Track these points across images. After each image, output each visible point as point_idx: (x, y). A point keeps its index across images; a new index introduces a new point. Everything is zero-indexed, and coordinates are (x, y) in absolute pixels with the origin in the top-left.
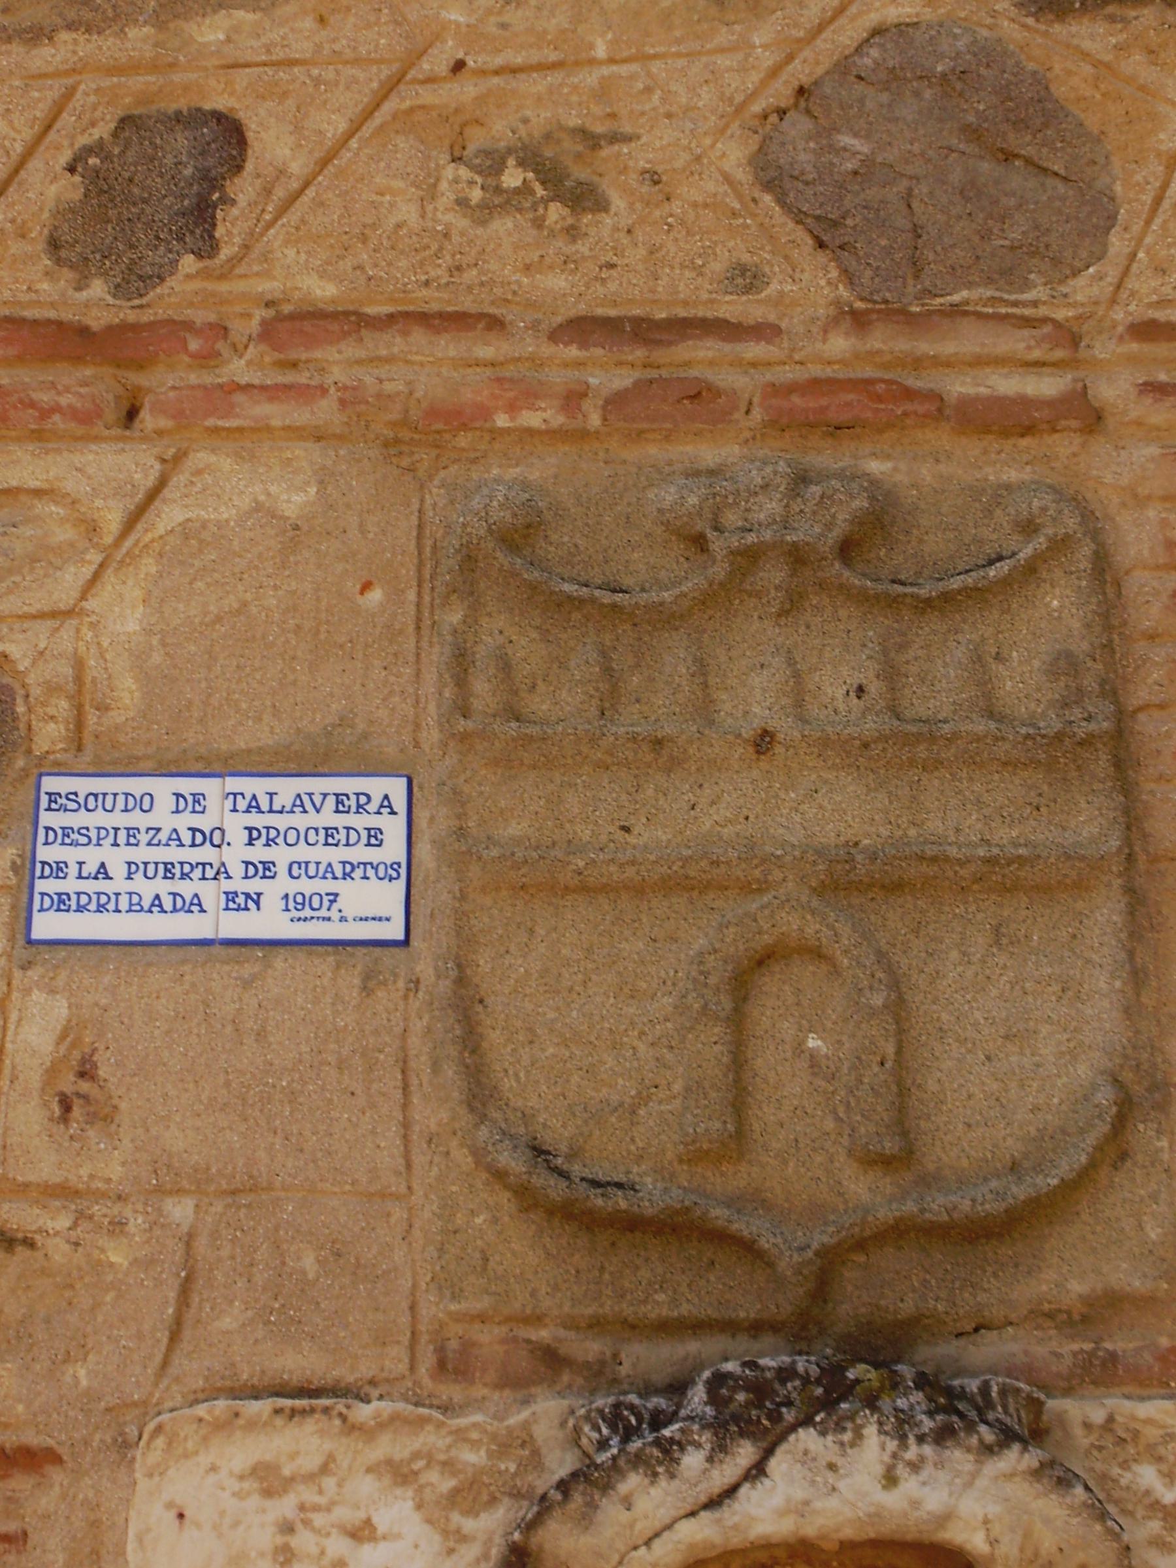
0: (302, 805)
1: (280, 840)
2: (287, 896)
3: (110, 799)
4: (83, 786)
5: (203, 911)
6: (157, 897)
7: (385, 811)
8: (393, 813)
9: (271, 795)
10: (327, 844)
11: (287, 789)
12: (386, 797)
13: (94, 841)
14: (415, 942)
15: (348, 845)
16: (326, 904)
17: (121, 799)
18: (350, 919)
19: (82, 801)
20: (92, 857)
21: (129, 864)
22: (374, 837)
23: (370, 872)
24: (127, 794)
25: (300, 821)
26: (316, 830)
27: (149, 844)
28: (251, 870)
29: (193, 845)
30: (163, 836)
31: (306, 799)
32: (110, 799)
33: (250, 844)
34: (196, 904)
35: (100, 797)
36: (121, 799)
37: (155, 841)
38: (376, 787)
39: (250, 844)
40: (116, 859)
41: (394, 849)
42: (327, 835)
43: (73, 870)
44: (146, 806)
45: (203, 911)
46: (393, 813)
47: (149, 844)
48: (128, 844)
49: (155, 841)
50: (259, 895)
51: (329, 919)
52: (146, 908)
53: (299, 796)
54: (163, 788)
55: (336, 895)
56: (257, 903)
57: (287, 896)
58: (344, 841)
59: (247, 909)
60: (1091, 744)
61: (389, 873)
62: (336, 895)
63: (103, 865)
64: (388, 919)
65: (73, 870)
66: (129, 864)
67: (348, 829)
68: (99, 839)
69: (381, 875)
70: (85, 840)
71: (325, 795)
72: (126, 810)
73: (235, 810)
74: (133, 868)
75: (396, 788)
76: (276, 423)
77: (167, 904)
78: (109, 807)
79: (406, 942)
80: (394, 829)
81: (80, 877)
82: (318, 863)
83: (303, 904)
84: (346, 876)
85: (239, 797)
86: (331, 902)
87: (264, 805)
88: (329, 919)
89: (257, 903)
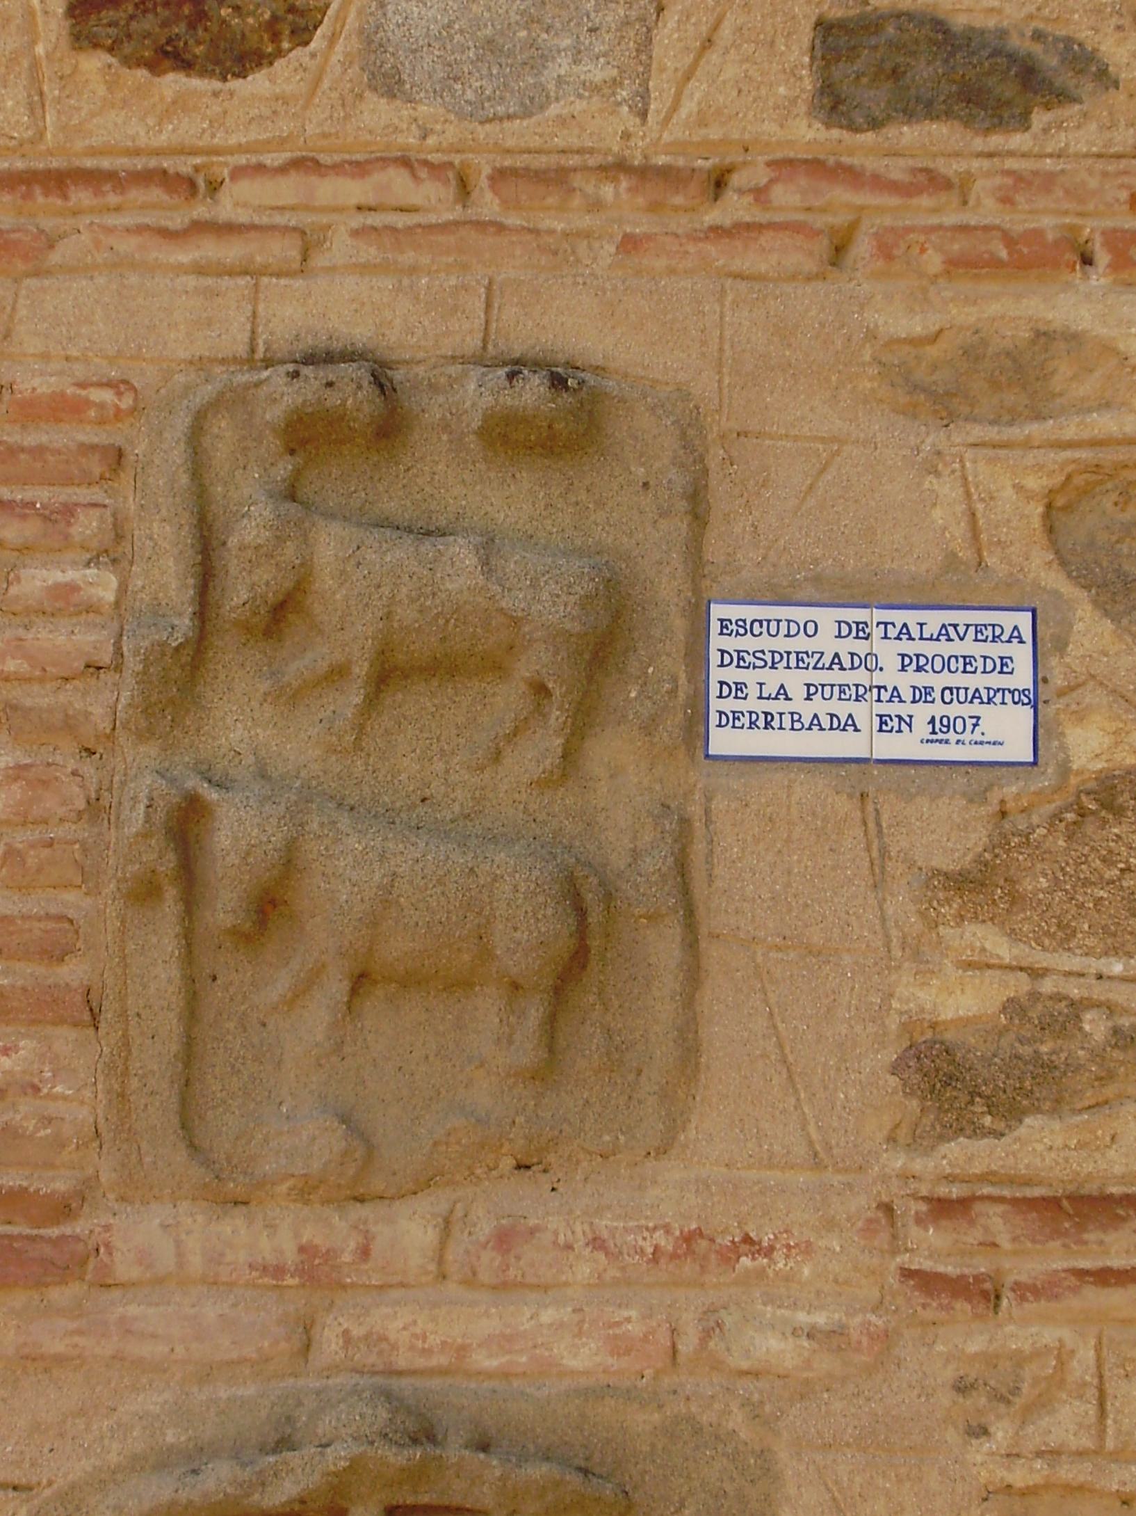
0: (947, 634)
1: (928, 667)
2: (933, 718)
3: (773, 625)
4: (750, 612)
5: (856, 730)
6: (815, 716)
7: (904, 637)
8: (1021, 642)
9: (921, 625)
10: (965, 671)
11: (934, 620)
12: (1016, 628)
13: (770, 664)
14: (1040, 761)
15: (984, 672)
16: (969, 727)
17: (783, 625)
18: (967, 742)
19: (748, 627)
20: (772, 680)
21: (808, 685)
22: (1004, 665)
23: (1008, 696)
24: (789, 621)
25: (945, 648)
26: (956, 657)
27: (815, 668)
28: (726, 690)
29: (852, 668)
30: (826, 660)
31: (951, 629)
32: (773, 625)
33: (903, 669)
34: (851, 723)
35: (765, 624)
36: (783, 625)
37: (820, 665)
38: (1007, 620)
39: (903, 669)
40: (795, 681)
41: (1022, 678)
42: (965, 664)
43: (753, 691)
44: (811, 632)
45: (856, 730)
46: (1021, 642)
47: (815, 668)
48: (798, 667)
49: (820, 665)
50: (911, 717)
51: (947, 742)
52: (807, 726)
53: (944, 626)
54: (827, 617)
55: (978, 718)
56: (910, 726)
57: (933, 718)
58: (980, 669)
59: (900, 731)
60: (308, 508)
61: (1018, 697)
62: (978, 718)
63: (782, 686)
64: (1001, 744)
65: (753, 691)
66: (808, 685)
67: (985, 658)
68: (773, 663)
69: (1016, 699)
70: (762, 663)
71: (968, 626)
72: (788, 635)
73: (886, 637)
74: (812, 690)
75: (1024, 621)
76: (400, 225)
77: (826, 723)
78: (773, 633)
79: (1035, 763)
80: (1022, 655)
81: (760, 698)
82: (966, 689)
83: (948, 727)
84: (990, 701)
85: (889, 627)
86: (975, 725)
87: (915, 633)
88: (947, 742)
89: (910, 726)
